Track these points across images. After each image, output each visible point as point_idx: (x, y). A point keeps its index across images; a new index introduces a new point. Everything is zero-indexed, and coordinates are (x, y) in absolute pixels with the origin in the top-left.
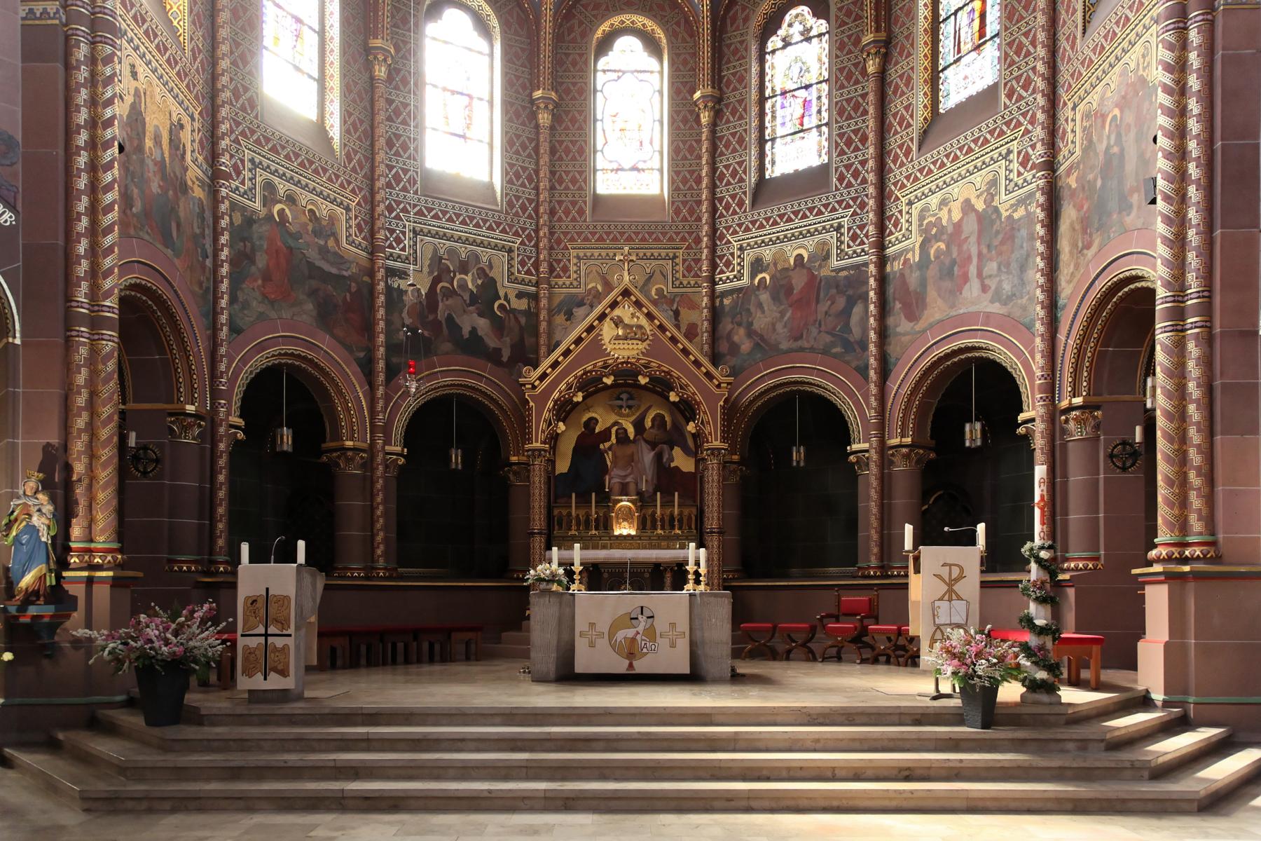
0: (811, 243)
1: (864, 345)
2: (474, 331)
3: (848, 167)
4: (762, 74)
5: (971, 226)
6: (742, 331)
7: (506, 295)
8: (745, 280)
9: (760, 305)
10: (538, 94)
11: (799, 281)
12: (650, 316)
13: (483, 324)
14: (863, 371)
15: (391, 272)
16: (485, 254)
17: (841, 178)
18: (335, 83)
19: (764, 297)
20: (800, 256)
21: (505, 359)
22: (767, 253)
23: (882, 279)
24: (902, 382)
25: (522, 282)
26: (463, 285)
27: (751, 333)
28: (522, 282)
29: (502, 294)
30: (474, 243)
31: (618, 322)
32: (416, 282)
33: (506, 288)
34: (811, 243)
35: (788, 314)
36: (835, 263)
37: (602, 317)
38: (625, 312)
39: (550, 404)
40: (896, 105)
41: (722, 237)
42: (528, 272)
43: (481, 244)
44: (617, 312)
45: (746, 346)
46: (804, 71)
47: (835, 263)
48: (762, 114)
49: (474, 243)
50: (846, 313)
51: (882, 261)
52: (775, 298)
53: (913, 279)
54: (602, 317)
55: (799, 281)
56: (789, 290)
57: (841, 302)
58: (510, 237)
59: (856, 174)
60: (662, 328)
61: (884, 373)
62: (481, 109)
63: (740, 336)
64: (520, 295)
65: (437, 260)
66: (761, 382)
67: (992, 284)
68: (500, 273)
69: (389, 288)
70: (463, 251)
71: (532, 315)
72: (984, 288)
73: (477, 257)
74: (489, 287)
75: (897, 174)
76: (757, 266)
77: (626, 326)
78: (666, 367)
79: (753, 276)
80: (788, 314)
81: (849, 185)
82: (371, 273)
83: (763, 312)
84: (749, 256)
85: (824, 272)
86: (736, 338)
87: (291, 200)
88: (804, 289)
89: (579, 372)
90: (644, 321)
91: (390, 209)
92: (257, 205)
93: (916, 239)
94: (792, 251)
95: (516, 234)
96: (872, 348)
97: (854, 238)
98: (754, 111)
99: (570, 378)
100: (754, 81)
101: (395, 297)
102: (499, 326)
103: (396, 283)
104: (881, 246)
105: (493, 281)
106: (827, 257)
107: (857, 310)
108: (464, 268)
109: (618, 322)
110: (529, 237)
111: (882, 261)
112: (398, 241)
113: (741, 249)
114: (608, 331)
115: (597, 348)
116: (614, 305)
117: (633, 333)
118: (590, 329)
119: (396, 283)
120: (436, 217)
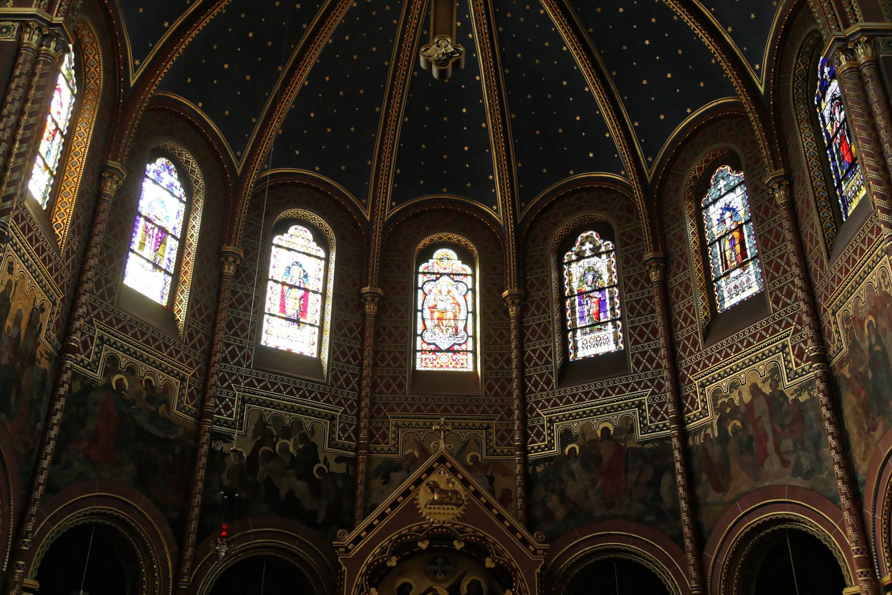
0: (616, 417)
1: (676, 513)
2: (291, 493)
3: (643, 354)
4: (561, 279)
5: (761, 407)
6: (555, 498)
7: (326, 459)
8: (556, 450)
9: (571, 473)
10: (367, 289)
11: (607, 452)
12: (465, 482)
13: (301, 486)
14: (678, 539)
15: (217, 436)
16: (308, 422)
17: (638, 363)
18: (187, 278)
19: (575, 466)
20: (606, 430)
21: (320, 521)
22: (576, 426)
23: (686, 452)
24: (719, 554)
25: (343, 447)
26: (285, 449)
27: (564, 499)
28: (343, 447)
29: (321, 457)
30: (299, 411)
31: (434, 487)
32: (240, 445)
33: (326, 452)
34: (616, 417)
35: (600, 483)
36: (639, 436)
37: (418, 482)
38: (441, 478)
39: (363, 568)
40: (680, 306)
41: (532, 410)
42: (349, 438)
43: (305, 412)
44: (433, 478)
45: (560, 513)
46: (597, 276)
47: (639, 436)
48: (563, 310)
49: (299, 411)
50: (655, 484)
51: (684, 435)
52: (586, 466)
53: (715, 452)
54: (418, 482)
55: (607, 452)
56: (599, 459)
57: (649, 473)
58: (333, 406)
59: (651, 360)
60: (477, 494)
61: (700, 542)
62: (314, 301)
63: (553, 502)
64: (339, 460)
65: (261, 425)
66: (579, 548)
67: (792, 459)
68: (322, 441)
69: (211, 451)
70: (288, 418)
71: (350, 479)
72: (785, 464)
73: (299, 424)
74: (310, 451)
75: (687, 361)
76: (567, 437)
77: (441, 492)
78: (481, 532)
79: (563, 446)
80: (600, 483)
81: (646, 369)
82: (196, 436)
83: (575, 480)
84: (558, 428)
85: (630, 444)
86: (550, 505)
87: (131, 371)
88: (611, 458)
89: (394, 536)
90: (459, 487)
91: (223, 380)
92: (98, 375)
93: (712, 417)
94: (599, 425)
95: (339, 404)
96: (685, 517)
97: (655, 414)
98: (556, 307)
99: (385, 542)
100: (554, 284)
101: (216, 459)
102: (316, 488)
103: (219, 446)
104: (681, 421)
105: (314, 447)
106: (632, 430)
107: (666, 480)
108: (287, 433)
109: (434, 487)
110: (351, 407)
111: (684, 435)
112: (227, 408)
113: (551, 421)
114: (424, 496)
115: (412, 512)
116: (430, 471)
117: (447, 498)
118: (406, 493)
119: (219, 446)
120: (265, 387)
